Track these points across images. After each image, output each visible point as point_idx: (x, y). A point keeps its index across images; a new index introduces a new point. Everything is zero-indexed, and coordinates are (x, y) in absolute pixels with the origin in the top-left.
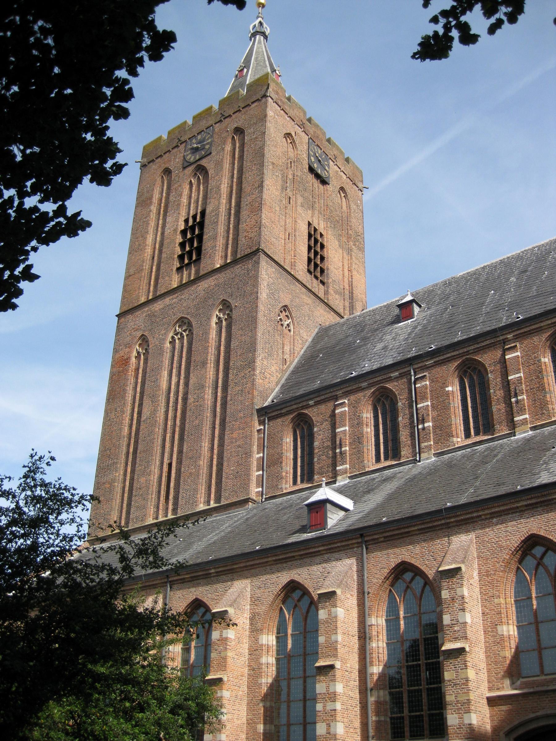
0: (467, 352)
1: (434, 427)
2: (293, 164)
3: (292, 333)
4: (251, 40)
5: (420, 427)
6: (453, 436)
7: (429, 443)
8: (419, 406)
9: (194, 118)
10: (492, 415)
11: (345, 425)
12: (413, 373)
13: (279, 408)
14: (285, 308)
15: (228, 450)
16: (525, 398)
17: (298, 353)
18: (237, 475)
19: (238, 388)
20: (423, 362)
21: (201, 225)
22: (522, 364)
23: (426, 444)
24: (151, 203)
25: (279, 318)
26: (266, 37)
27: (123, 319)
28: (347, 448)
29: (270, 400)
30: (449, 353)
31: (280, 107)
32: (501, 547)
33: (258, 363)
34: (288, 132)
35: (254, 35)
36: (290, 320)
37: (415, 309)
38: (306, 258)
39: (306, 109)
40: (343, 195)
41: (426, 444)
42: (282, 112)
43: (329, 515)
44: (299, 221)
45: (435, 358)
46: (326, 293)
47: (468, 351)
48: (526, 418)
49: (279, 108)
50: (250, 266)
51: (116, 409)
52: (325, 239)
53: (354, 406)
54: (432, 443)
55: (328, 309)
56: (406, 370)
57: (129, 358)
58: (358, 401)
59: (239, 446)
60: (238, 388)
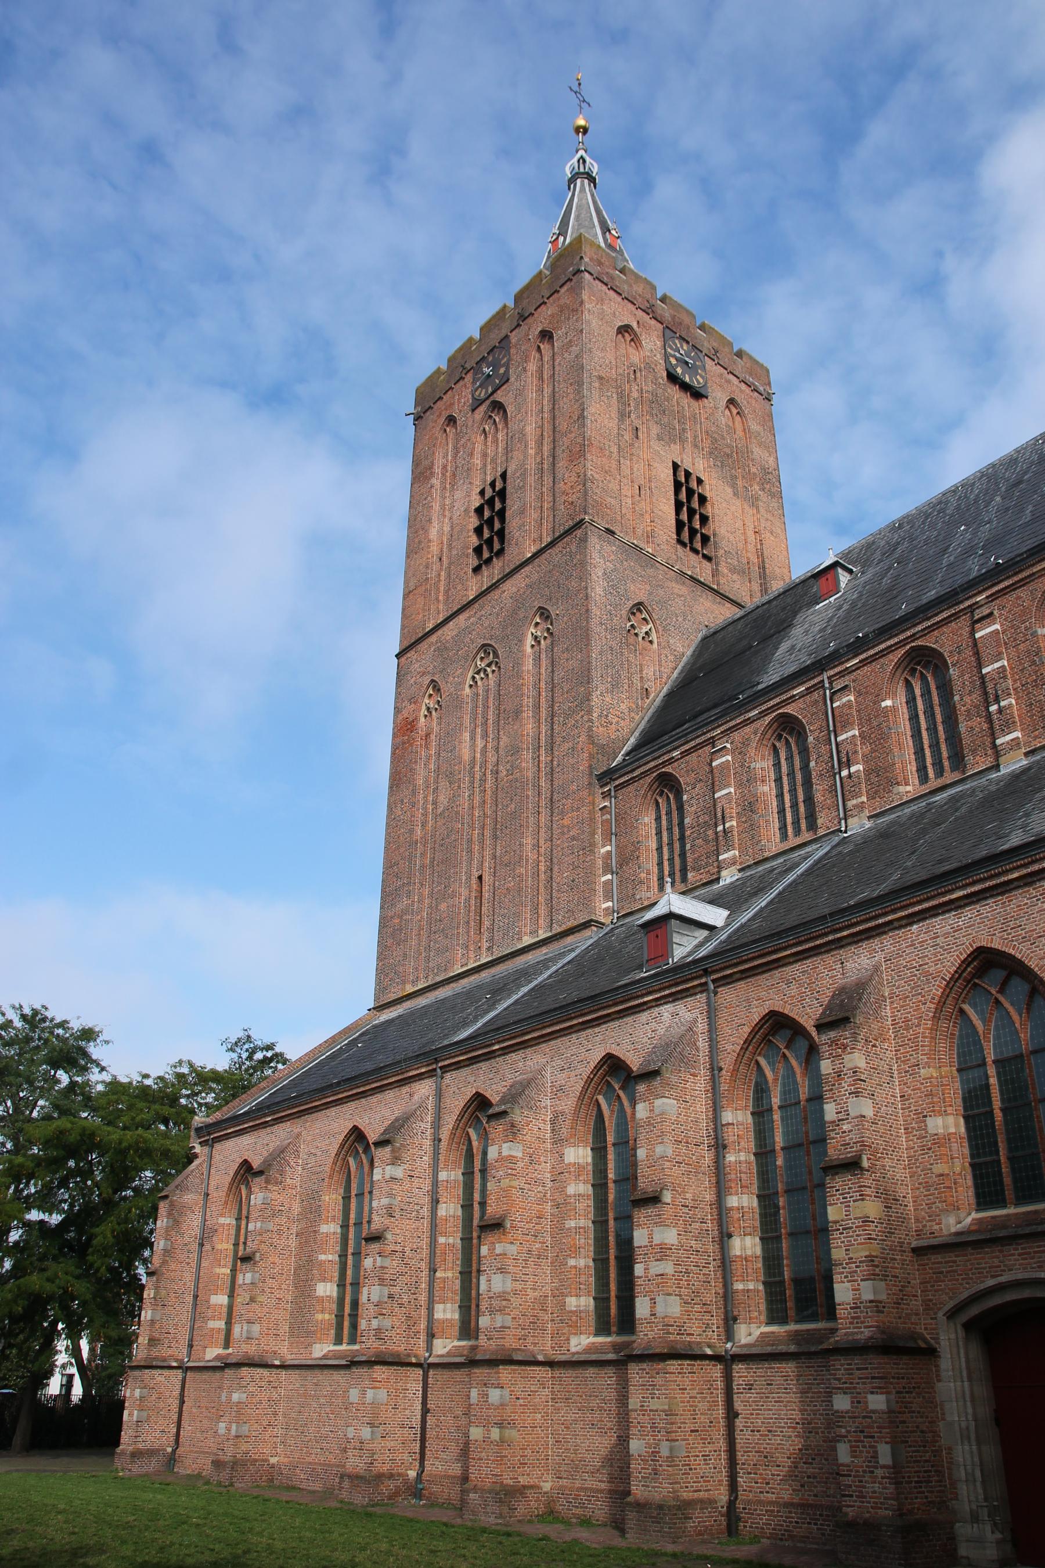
0: (911, 636)
1: (868, 772)
2: (638, 374)
3: (655, 645)
4: (569, 189)
5: (845, 773)
6: (898, 784)
7: (860, 800)
8: (839, 739)
9: (481, 329)
10: (961, 740)
11: (728, 786)
12: (827, 685)
13: (629, 768)
14: (639, 607)
15: (558, 846)
16: (1013, 702)
17: (669, 677)
18: (572, 886)
19: (567, 745)
20: (843, 663)
21: (502, 494)
22: (1005, 644)
23: (854, 802)
24: (432, 474)
25: (629, 624)
26: (592, 180)
27: (403, 659)
28: (734, 823)
29: (620, 758)
30: (882, 643)
31: (606, 285)
32: (927, 974)
33: (595, 700)
34: (626, 323)
35: (572, 181)
36: (651, 625)
37: (841, 578)
38: (674, 522)
39: (655, 282)
40: (735, 411)
41: (854, 802)
42: (611, 293)
43: (676, 938)
44: (656, 465)
45: (861, 654)
46: (715, 573)
47: (914, 635)
48: (1018, 738)
49: (604, 288)
50: (574, 548)
51: (402, 801)
52: (707, 487)
53: (740, 752)
54: (864, 799)
55: (718, 599)
56: (816, 681)
57: (416, 719)
58: (746, 743)
59: (573, 838)
60: (567, 745)
